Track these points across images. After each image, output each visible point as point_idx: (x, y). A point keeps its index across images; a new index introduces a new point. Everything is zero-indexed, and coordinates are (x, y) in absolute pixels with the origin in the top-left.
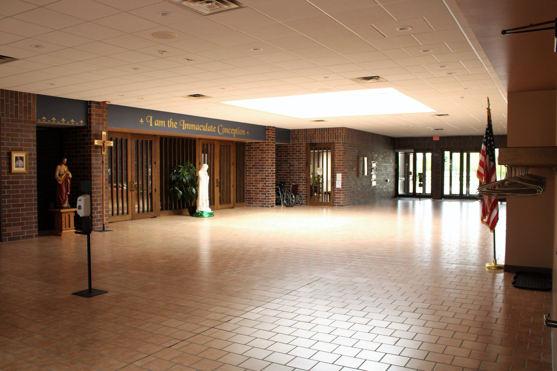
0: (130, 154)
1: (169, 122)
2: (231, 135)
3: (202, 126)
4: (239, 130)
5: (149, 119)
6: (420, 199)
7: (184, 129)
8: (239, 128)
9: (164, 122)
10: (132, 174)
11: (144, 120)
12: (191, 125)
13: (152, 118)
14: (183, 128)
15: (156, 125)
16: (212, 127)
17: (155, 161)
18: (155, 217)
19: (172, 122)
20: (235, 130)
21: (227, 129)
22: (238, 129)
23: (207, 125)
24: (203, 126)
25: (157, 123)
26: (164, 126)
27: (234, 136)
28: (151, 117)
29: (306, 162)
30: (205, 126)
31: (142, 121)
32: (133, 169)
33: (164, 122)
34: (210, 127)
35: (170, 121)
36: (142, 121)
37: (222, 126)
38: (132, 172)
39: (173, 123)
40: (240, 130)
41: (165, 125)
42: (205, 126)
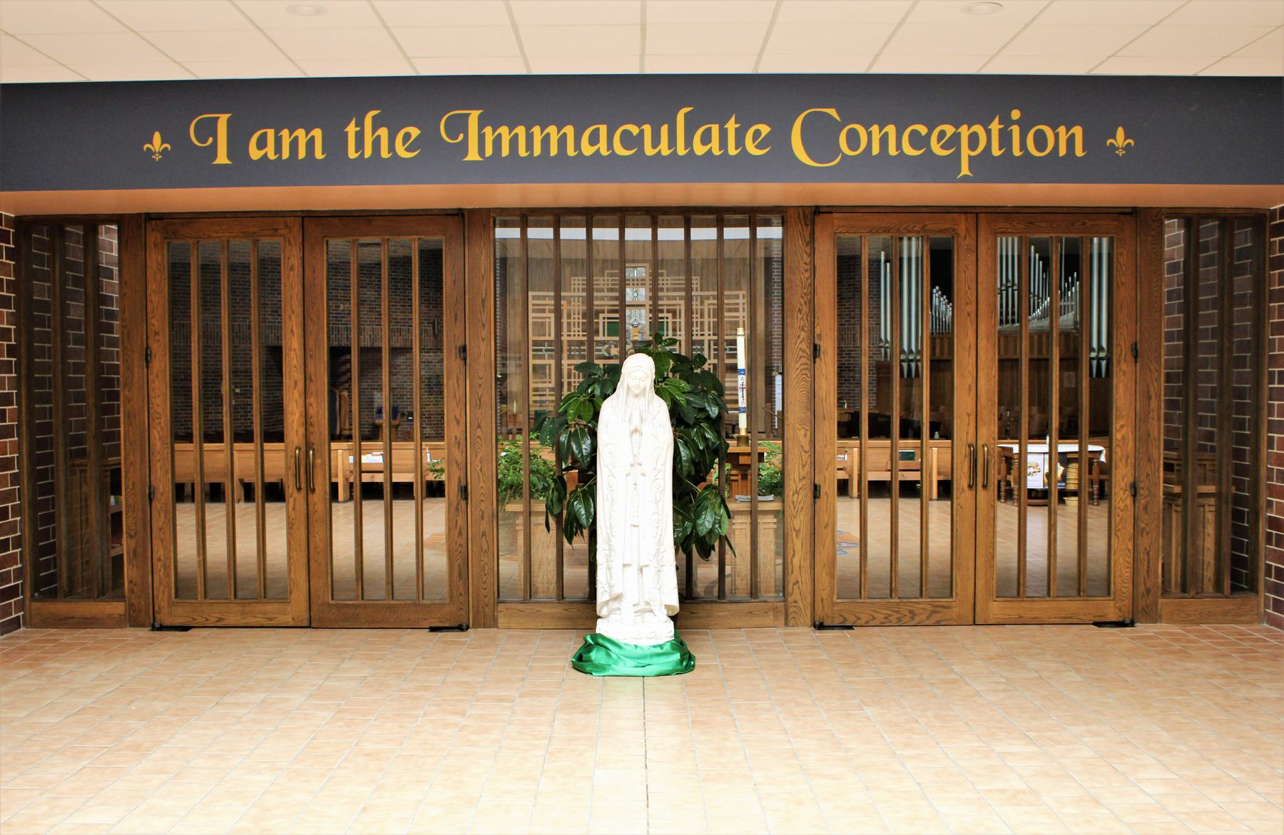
0: (299, 311)
1: (351, 129)
2: (945, 169)
3: (634, 130)
4: (1015, 129)
5: (208, 129)
6: (599, 617)
7: (473, 155)
8: (1016, 114)
9: (317, 133)
10: (311, 411)
11: (175, 136)
12: (1062, 130)
13: (230, 123)
14: (215, 156)
15: (255, 154)
16: (731, 126)
17: (460, 343)
18: (461, 628)
19: (374, 130)
20: (978, 128)
21: (891, 129)
22: (1007, 121)
23: (374, 118)
24: (647, 129)
25: (262, 144)
26: (1079, 152)
27: (965, 170)
28: (223, 119)
29: (1187, 303)
30: (664, 130)
31: (157, 143)
32: (312, 387)
33: (317, 133)
34: (715, 129)
35: (360, 124)
36: (157, 143)
37: (832, 112)
38: (312, 400)
39: (383, 132)
40: (1025, 127)
41: (324, 151)
42: (664, 130)
